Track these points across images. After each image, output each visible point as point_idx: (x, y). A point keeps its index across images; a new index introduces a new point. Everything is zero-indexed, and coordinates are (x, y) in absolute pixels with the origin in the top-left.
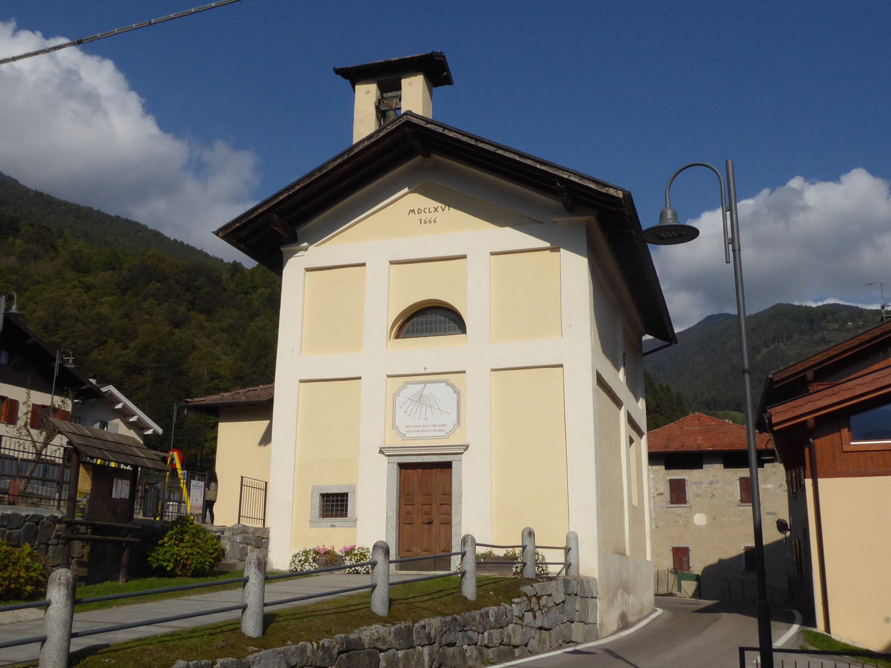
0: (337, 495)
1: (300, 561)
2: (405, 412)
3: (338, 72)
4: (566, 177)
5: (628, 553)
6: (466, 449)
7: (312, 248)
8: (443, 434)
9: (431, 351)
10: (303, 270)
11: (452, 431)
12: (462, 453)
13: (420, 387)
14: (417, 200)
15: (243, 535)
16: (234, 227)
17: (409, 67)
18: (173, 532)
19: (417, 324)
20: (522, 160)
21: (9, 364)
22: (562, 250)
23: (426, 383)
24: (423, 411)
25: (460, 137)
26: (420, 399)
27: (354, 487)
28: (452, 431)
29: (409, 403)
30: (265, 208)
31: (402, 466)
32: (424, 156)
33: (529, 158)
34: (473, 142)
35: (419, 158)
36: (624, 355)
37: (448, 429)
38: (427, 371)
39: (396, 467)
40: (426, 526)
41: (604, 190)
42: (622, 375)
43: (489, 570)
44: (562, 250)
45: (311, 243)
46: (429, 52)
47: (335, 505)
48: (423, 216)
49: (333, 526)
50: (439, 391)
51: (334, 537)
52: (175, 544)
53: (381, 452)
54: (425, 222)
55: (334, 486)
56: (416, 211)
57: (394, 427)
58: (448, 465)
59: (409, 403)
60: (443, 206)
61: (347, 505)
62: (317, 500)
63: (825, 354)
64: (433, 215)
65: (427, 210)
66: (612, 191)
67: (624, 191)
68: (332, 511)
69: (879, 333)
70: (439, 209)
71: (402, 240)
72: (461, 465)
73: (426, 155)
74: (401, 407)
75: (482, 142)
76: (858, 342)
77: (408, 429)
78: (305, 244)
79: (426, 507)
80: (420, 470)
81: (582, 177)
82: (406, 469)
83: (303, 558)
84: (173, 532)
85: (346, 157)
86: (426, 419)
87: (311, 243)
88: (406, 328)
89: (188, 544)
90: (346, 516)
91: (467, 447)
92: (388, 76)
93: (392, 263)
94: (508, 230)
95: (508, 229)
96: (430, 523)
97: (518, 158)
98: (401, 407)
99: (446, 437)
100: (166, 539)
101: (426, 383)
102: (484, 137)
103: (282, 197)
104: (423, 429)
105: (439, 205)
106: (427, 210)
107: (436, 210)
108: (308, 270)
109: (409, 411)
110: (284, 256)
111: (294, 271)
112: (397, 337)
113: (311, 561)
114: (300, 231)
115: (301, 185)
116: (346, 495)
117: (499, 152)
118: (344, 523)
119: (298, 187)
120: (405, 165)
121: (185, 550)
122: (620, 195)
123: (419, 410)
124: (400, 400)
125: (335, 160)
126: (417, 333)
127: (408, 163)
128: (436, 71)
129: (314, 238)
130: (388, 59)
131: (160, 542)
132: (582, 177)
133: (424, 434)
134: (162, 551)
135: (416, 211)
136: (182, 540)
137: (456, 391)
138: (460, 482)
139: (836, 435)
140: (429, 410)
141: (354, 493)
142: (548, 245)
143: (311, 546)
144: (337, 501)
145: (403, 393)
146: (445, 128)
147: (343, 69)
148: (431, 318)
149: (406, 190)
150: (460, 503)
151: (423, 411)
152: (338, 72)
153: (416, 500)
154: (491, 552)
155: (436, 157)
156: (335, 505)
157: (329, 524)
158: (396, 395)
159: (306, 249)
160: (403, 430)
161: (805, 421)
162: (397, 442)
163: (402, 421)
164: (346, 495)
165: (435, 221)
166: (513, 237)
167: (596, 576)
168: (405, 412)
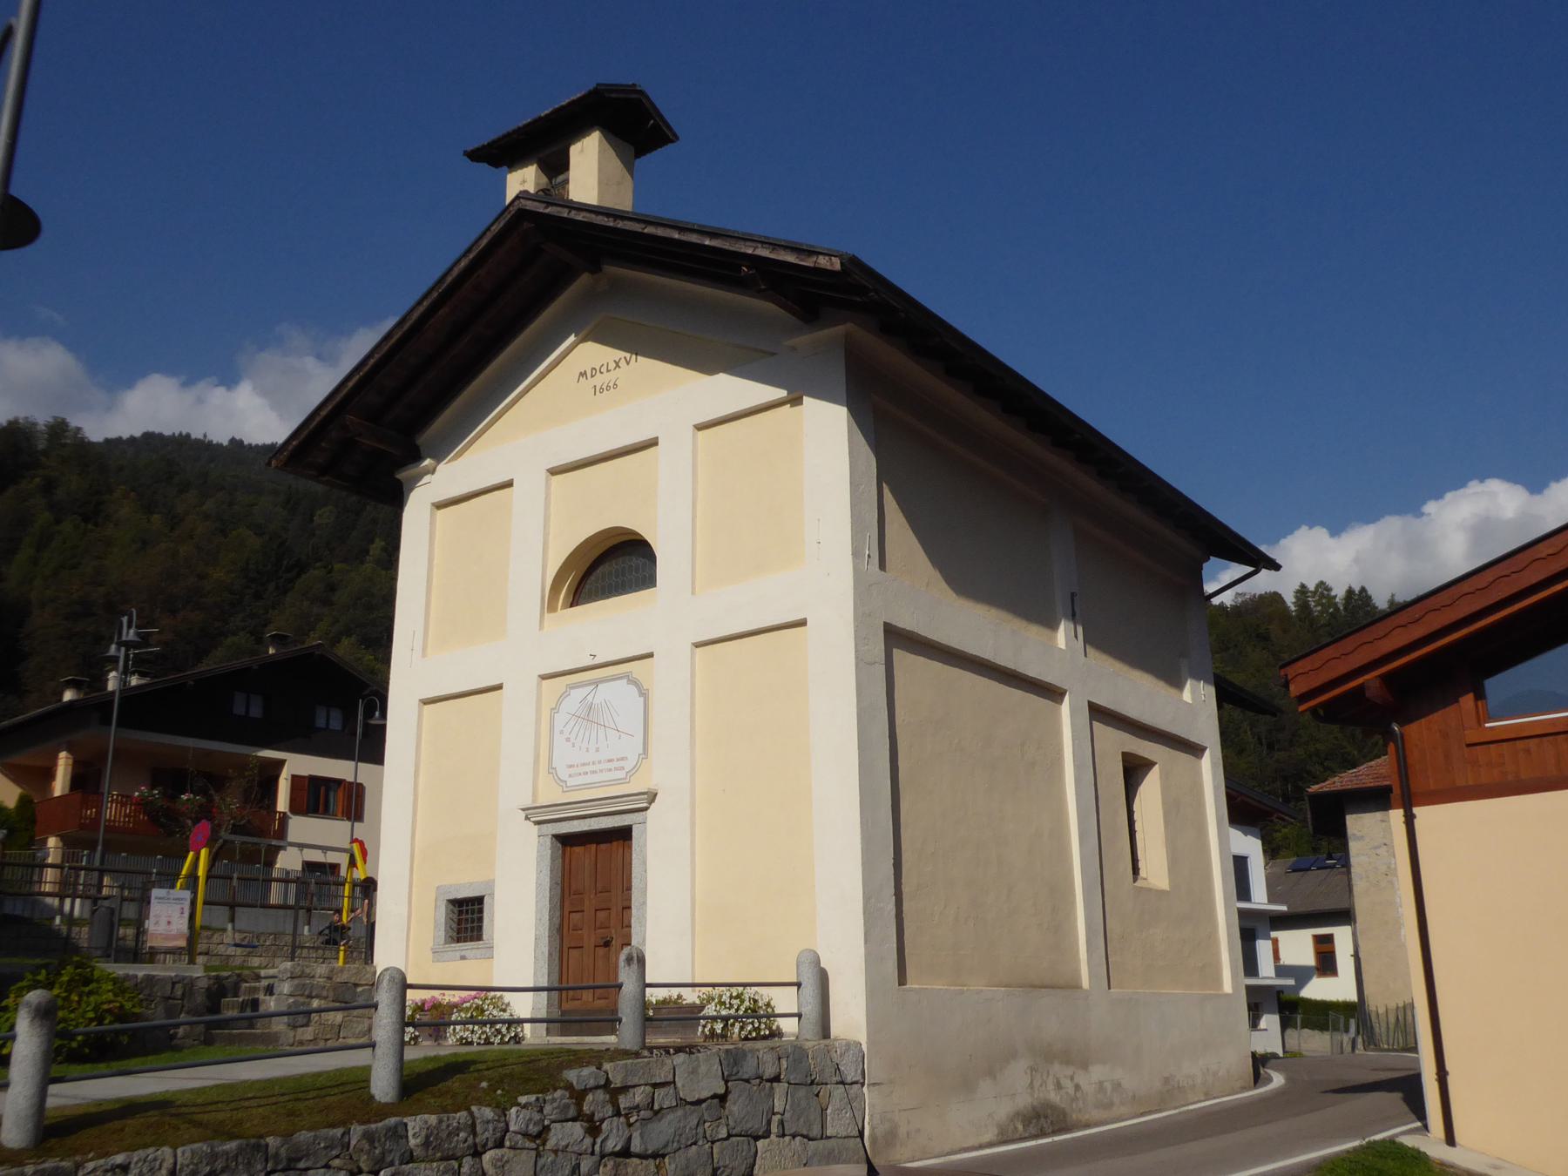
2: (568, 740)
3: (475, 155)
4: (750, 251)
5: (1085, 983)
7: (442, 467)
8: (621, 774)
9: (612, 622)
11: (636, 769)
12: (646, 809)
14: (591, 354)
15: (296, 981)
21: (344, 727)
22: (805, 399)
23: (596, 683)
26: (589, 715)
27: (490, 884)
28: (636, 769)
31: (566, 841)
32: (593, 272)
33: (692, 231)
35: (584, 279)
36: (1073, 595)
37: (629, 765)
38: (597, 661)
39: (548, 840)
40: (601, 951)
41: (809, 262)
42: (1063, 636)
43: (666, 1034)
44: (805, 399)
45: (439, 457)
46: (591, 87)
47: (466, 918)
48: (599, 380)
49: (463, 958)
50: (616, 695)
58: (625, 834)
59: (572, 723)
60: (628, 355)
66: (823, 262)
67: (840, 256)
70: (623, 363)
73: (595, 268)
77: (572, 771)
78: (427, 462)
79: (601, 915)
80: (594, 846)
81: (775, 246)
88: (586, 590)
90: (479, 938)
91: (652, 797)
94: (723, 379)
101: (596, 683)
102: (729, 227)
103: (350, 384)
104: (591, 768)
112: (574, 603)
114: (422, 440)
117: (649, 230)
120: (826, 331)
122: (836, 265)
124: (560, 719)
125: (419, 303)
128: (634, 125)
130: (535, 116)
132: (775, 246)
133: (587, 778)
137: (644, 694)
139: (1451, 709)
142: (781, 393)
146: (682, 229)
147: (478, 149)
148: (613, 564)
149: (572, 338)
152: (475, 155)
153: (587, 902)
154: (680, 997)
155: (612, 270)
157: (458, 954)
159: (433, 472)
160: (563, 773)
161: (1361, 687)
162: (550, 794)
166: (732, 391)
167: (862, 1038)
168: (568, 740)
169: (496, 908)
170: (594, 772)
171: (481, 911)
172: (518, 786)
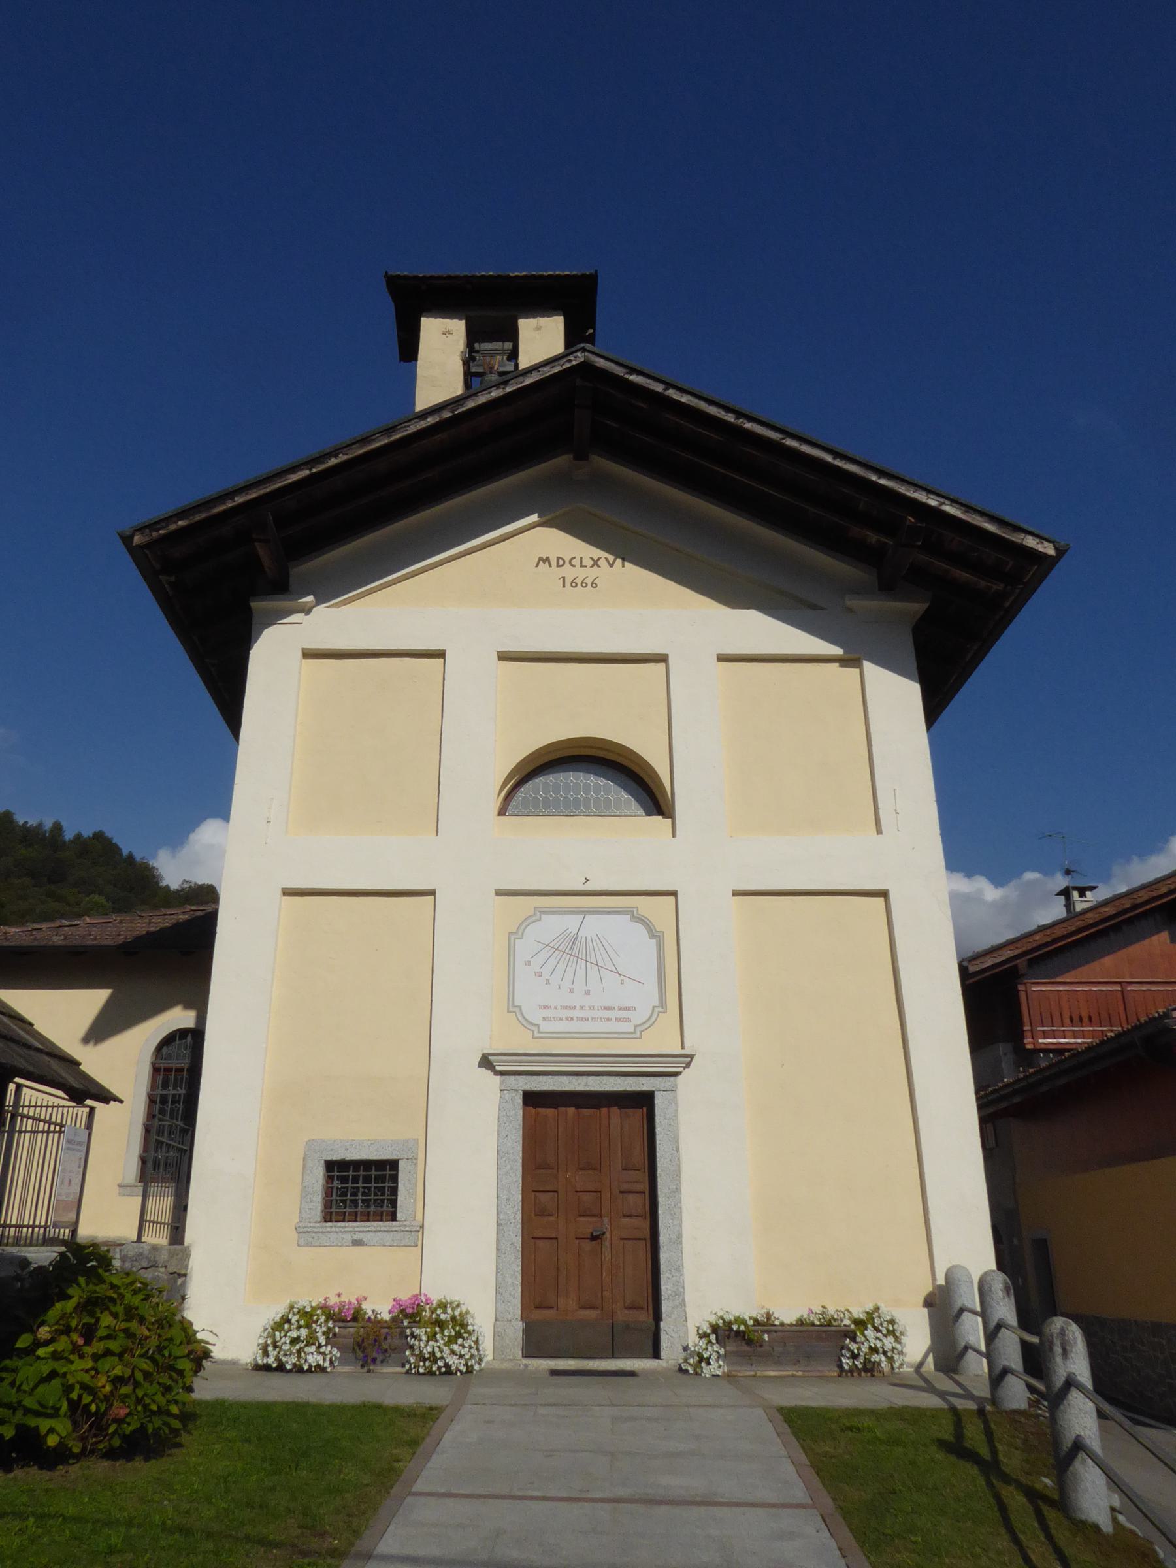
0: (367, 1164)
1: (294, 1341)
2: (539, 974)
6: (688, 1065)
7: (320, 610)
9: (599, 842)
10: (300, 653)
11: (649, 1023)
13: (571, 922)
16: (173, 527)
17: (540, 296)
18: (70, 1305)
19: (567, 788)
20: (838, 462)
24: (581, 973)
25: (703, 405)
26: (572, 946)
28: (649, 1023)
29: (544, 954)
30: (253, 495)
31: (531, 1099)
34: (730, 418)
35: (562, 461)
37: (639, 1017)
38: (589, 887)
40: (587, 1246)
47: (362, 1189)
48: (569, 572)
49: (357, 1243)
50: (611, 930)
51: (368, 1273)
52: (76, 1349)
53: (486, 1062)
54: (574, 584)
55: (362, 1141)
56: (554, 562)
57: (512, 1007)
59: (544, 954)
60: (611, 558)
61: (394, 1191)
62: (320, 1173)
63: (1048, 932)
64: (591, 573)
65: (576, 562)
68: (355, 1202)
69: (1128, 906)
70: (602, 562)
71: (516, 614)
72: (674, 1101)
74: (528, 963)
75: (751, 419)
76: (1098, 917)
77: (546, 1013)
78: (310, 599)
82: (536, 1106)
83: (304, 1332)
84: (70, 1305)
85: (447, 414)
86: (587, 993)
87: (318, 602)
89: (114, 1346)
92: (491, 310)
93: (504, 657)
95: (752, 611)
96: (593, 1238)
97: (829, 458)
98: (528, 963)
99: (638, 1032)
100: (44, 1332)
105: (597, 553)
106: (576, 562)
107: (596, 563)
108: (309, 654)
109: (546, 972)
110: (255, 620)
111: (276, 657)
113: (323, 1341)
114: (299, 571)
115: (342, 458)
116: (393, 1165)
117: (790, 442)
118: (387, 1237)
119: (333, 461)
121: (105, 1364)
123: (570, 970)
124: (524, 948)
126: (567, 807)
127: (546, 464)
128: (574, 300)
129: (330, 589)
131: (23, 1341)
133: (592, 1021)
134: (28, 1372)
135: (554, 562)
136: (89, 1334)
138: (676, 1140)
140: (593, 971)
141: (413, 1160)
142: (837, 651)
143: (308, 1299)
144: (367, 1179)
145: (532, 931)
149: (534, 518)
150: (678, 1190)
151: (581, 973)
155: (601, 463)
156: (362, 1189)
157: (349, 1237)
158: (515, 935)
159: (307, 611)
160: (535, 1016)
163: (530, 994)
164: (393, 1165)
165: (594, 584)
169: (683, 1118)
170: (583, 1019)
171: (395, 1179)
172: (470, 1021)
